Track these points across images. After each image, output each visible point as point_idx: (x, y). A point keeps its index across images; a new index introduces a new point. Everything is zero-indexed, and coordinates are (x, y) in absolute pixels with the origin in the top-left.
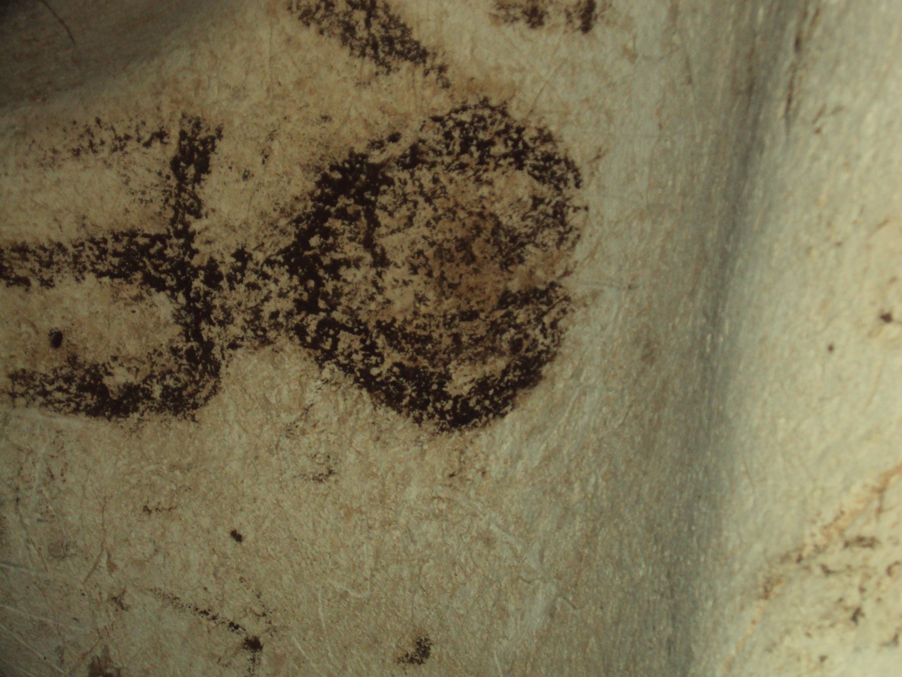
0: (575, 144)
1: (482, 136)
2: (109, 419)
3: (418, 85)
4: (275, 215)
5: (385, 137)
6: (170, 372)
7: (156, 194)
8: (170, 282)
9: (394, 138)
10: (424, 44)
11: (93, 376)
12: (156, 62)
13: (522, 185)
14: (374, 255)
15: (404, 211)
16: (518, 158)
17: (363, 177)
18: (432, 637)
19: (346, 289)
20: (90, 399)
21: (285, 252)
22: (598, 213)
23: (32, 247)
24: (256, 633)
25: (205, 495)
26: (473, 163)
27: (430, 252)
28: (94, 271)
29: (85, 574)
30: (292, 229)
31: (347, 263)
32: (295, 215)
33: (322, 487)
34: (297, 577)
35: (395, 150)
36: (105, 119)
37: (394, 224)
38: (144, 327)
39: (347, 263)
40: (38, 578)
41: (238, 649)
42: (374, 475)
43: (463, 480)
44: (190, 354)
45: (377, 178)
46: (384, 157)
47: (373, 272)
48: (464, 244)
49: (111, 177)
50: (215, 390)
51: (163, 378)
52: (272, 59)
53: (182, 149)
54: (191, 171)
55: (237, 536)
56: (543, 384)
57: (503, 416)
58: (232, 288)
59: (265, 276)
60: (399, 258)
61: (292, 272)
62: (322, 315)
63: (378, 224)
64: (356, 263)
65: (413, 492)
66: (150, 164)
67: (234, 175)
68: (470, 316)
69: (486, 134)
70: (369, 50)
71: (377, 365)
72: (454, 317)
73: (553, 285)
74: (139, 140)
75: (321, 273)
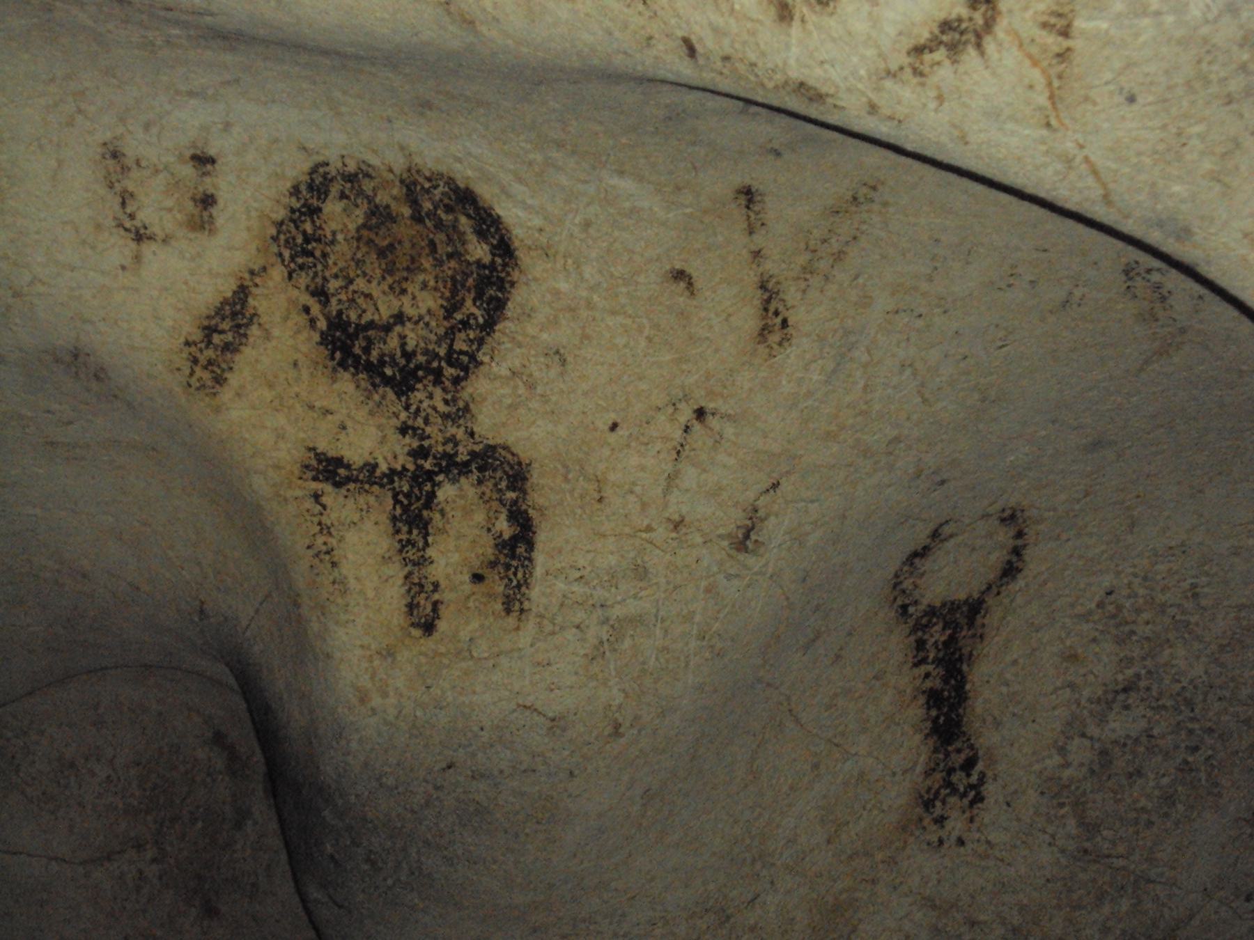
0: (297, 168)
1: (300, 240)
2: (534, 533)
3: (266, 291)
4: (371, 404)
5: (306, 317)
6: (496, 485)
7: (362, 500)
8: (428, 487)
9: (307, 310)
10: (234, 288)
11: (504, 547)
12: (263, 503)
13: (333, 207)
14: (395, 324)
15: (361, 301)
16: (314, 212)
17: (338, 334)
18: (668, 267)
19: (422, 345)
20: (521, 550)
21: (399, 394)
22: (345, 148)
23: (409, 600)
24: (690, 412)
25: (587, 454)
26: (321, 246)
27: (390, 280)
28: (424, 550)
29: (658, 551)
30: (381, 390)
31: (403, 345)
32: (370, 387)
33: (570, 359)
34: (641, 378)
35: (316, 309)
36: (307, 542)
37: (371, 309)
38: (464, 508)
39: (403, 345)
40: (665, 591)
41: (706, 426)
42: (556, 317)
43: (549, 247)
44: (481, 469)
45: (338, 323)
46: (321, 317)
47: (409, 325)
48: (382, 253)
49: (351, 537)
50: (506, 448)
51: (501, 490)
52: (253, 408)
53: (327, 479)
54: (342, 471)
55: (614, 427)
56: (472, 186)
57: (499, 217)
58: (429, 437)
59: (418, 410)
60: (396, 303)
61: (413, 389)
62: (443, 364)
63: (372, 322)
64: (403, 337)
65: (563, 286)
66: (341, 505)
67: (342, 437)
68: (432, 245)
69: (297, 236)
70: (242, 331)
71: (476, 319)
72: (435, 259)
73: (402, 181)
74: (321, 514)
75: (412, 366)
